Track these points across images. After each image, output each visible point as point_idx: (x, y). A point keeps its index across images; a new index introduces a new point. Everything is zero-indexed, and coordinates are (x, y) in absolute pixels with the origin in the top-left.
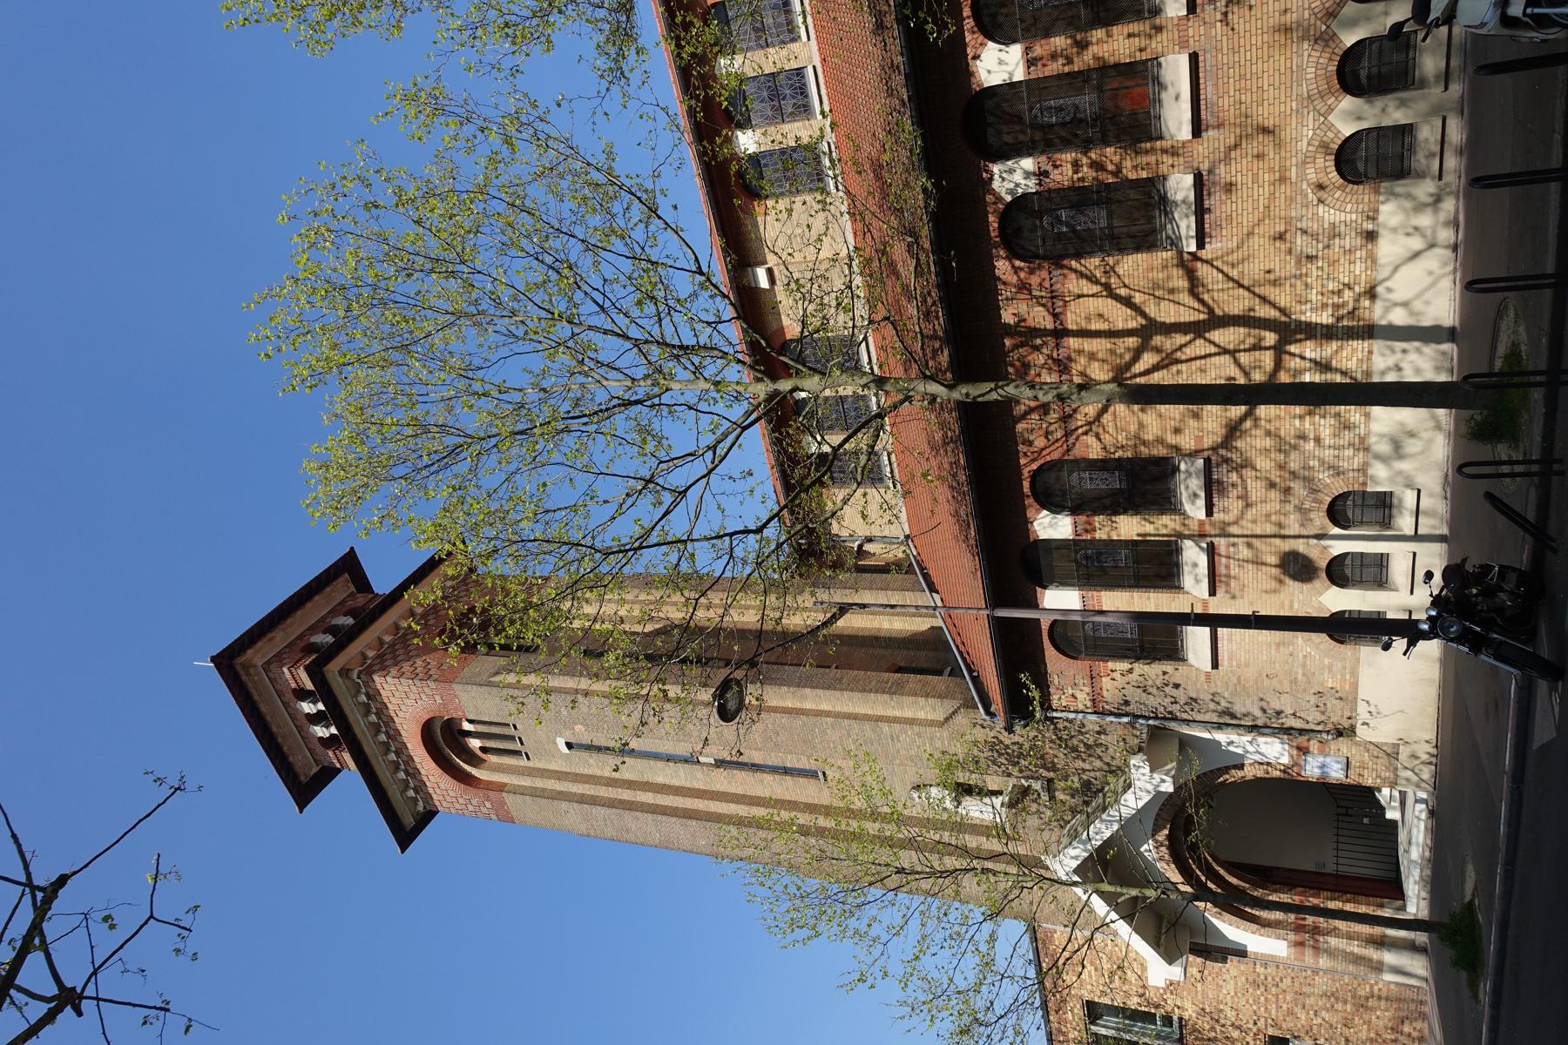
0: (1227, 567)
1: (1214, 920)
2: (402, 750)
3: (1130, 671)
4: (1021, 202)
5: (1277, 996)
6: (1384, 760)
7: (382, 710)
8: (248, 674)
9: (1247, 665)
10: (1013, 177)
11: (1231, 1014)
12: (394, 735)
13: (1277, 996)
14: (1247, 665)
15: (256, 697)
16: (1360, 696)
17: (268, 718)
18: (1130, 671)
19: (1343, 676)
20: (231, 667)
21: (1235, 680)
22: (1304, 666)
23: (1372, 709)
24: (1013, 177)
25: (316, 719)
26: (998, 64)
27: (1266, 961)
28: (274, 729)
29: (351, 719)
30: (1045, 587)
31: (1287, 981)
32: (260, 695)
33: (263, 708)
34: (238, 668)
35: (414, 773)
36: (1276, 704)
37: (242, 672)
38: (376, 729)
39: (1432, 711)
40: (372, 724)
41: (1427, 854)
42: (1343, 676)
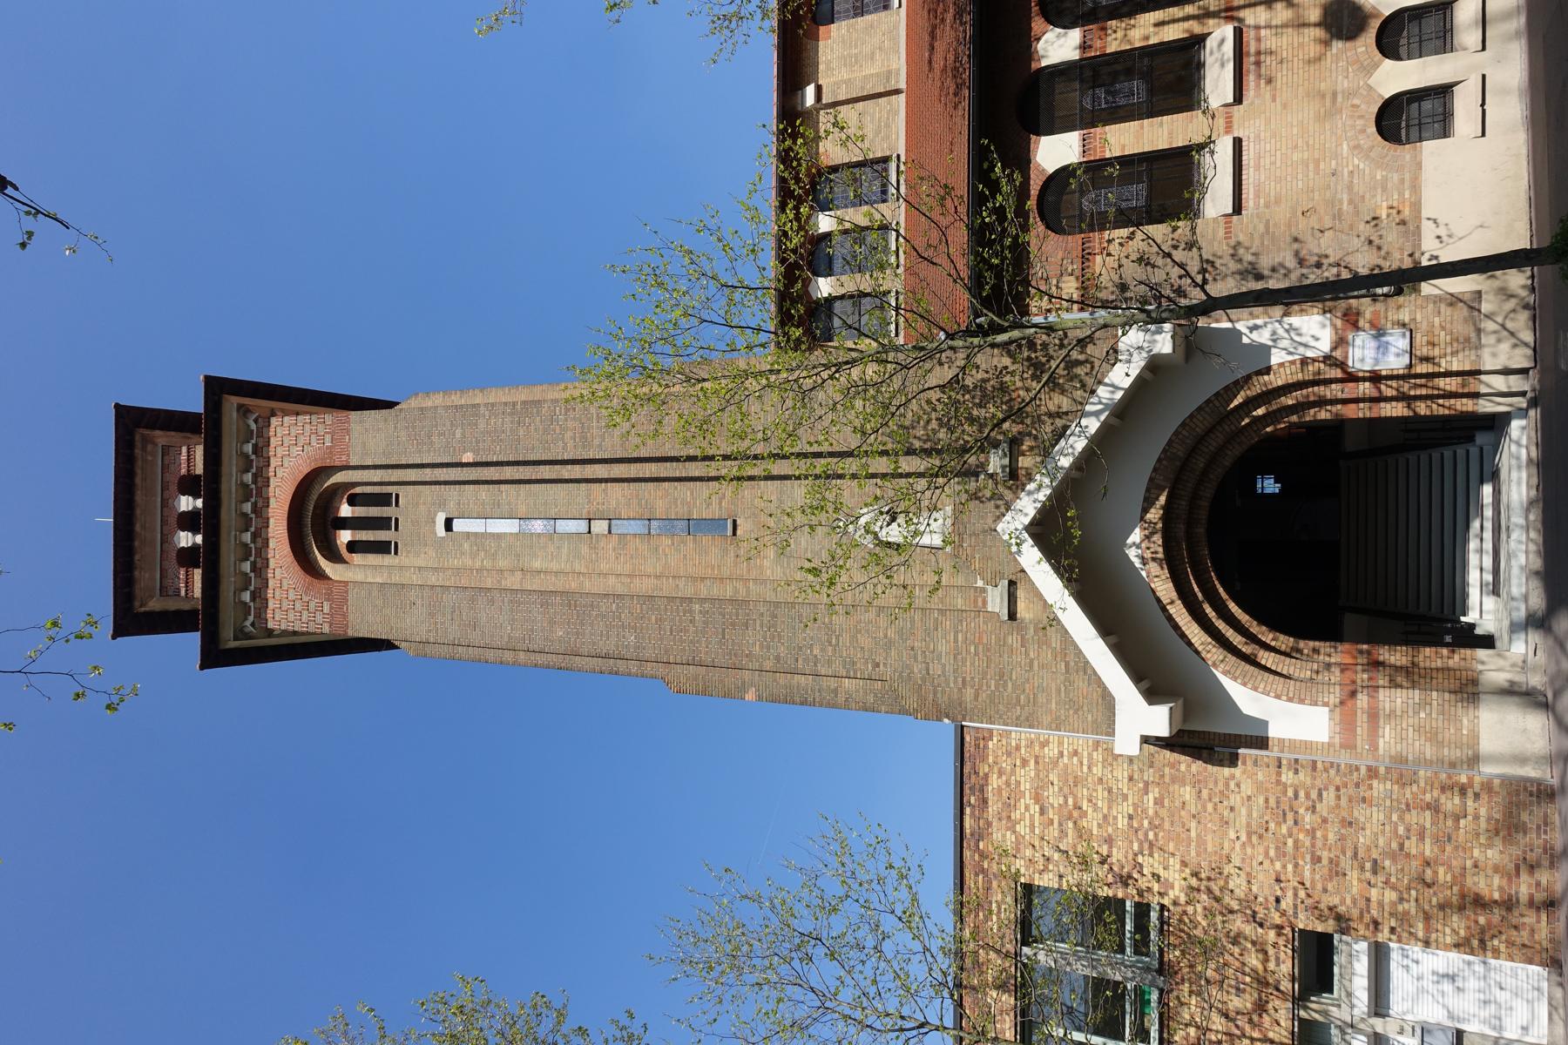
0: (1258, 40)
1: (1226, 682)
2: (261, 510)
3: (1131, 237)
4: (1065, 173)
5: (1312, 833)
6: (1462, 311)
7: (261, 449)
8: (144, 449)
9: (1278, 201)
10: (1055, 151)
11: (1238, 883)
12: (262, 480)
13: (1312, 833)
14: (1278, 201)
15: (138, 480)
16: (1424, 214)
17: (138, 512)
18: (1131, 237)
19: (1401, 194)
20: (132, 434)
21: (1261, 228)
22: (1350, 187)
23: (1442, 232)
24: (1055, 151)
25: (189, 521)
26: (1058, 46)
27: (1302, 758)
28: (138, 528)
29: (225, 469)
30: (1039, 134)
31: (1329, 796)
32: (143, 527)
33: (139, 497)
34: (137, 437)
35: (261, 536)
36: (1312, 247)
37: (138, 444)
38: (246, 522)
39: (1523, 204)
40: (245, 486)
41: (1533, 493)
42: (1401, 194)
